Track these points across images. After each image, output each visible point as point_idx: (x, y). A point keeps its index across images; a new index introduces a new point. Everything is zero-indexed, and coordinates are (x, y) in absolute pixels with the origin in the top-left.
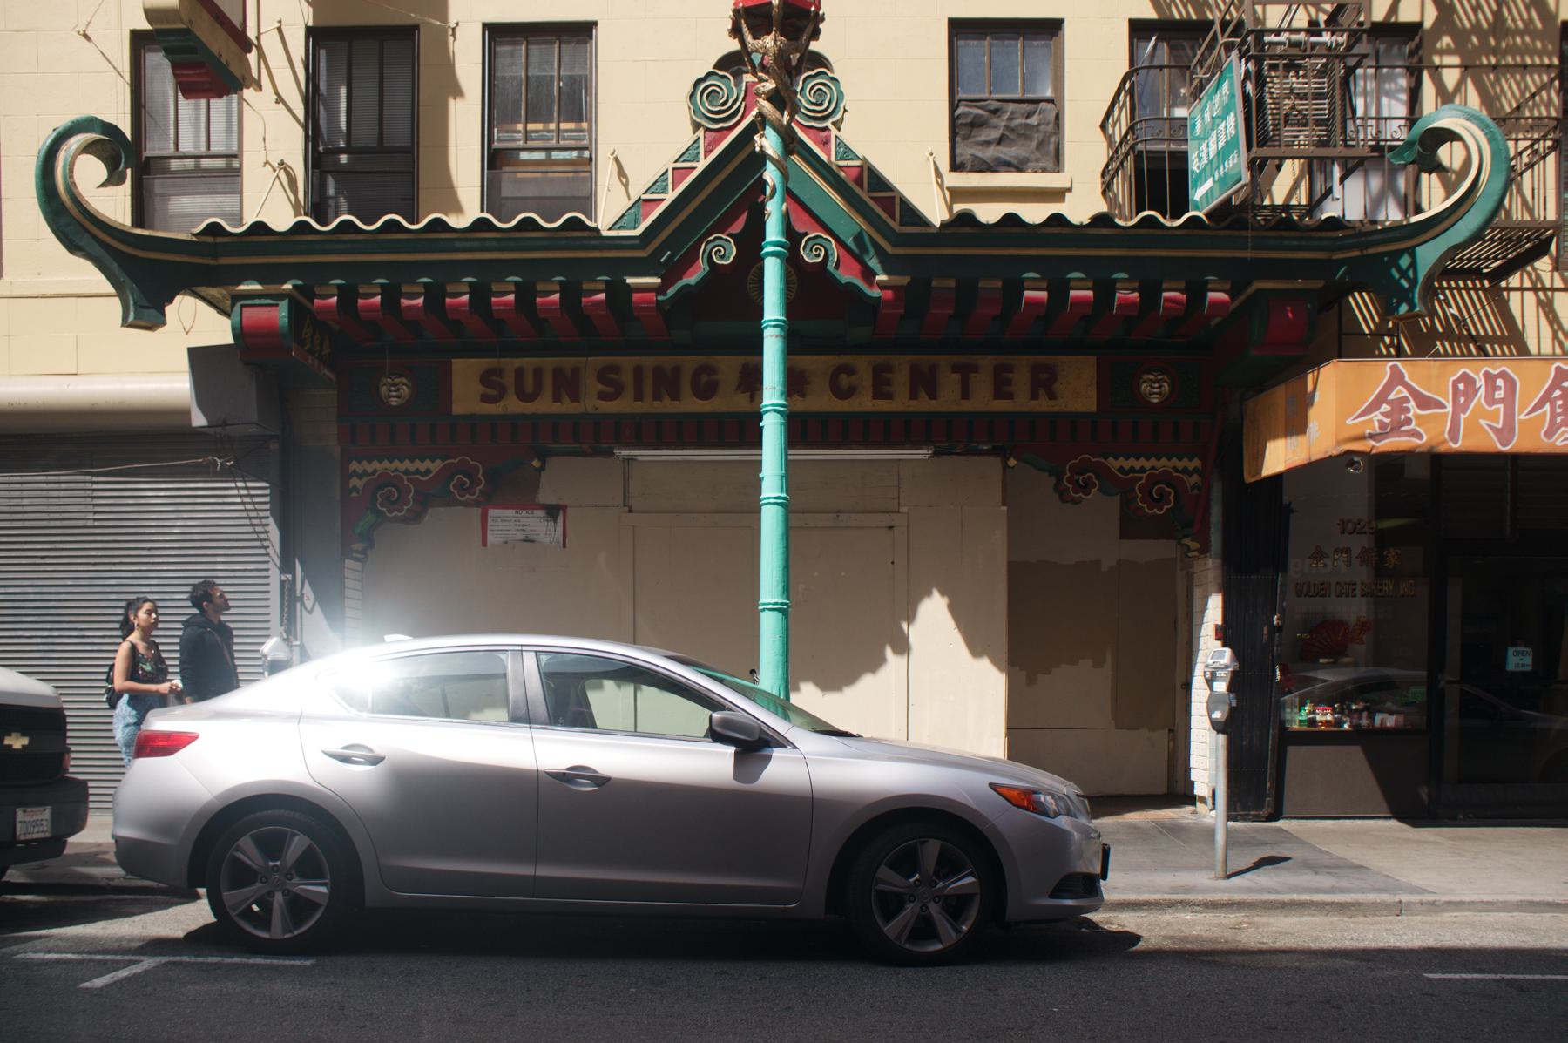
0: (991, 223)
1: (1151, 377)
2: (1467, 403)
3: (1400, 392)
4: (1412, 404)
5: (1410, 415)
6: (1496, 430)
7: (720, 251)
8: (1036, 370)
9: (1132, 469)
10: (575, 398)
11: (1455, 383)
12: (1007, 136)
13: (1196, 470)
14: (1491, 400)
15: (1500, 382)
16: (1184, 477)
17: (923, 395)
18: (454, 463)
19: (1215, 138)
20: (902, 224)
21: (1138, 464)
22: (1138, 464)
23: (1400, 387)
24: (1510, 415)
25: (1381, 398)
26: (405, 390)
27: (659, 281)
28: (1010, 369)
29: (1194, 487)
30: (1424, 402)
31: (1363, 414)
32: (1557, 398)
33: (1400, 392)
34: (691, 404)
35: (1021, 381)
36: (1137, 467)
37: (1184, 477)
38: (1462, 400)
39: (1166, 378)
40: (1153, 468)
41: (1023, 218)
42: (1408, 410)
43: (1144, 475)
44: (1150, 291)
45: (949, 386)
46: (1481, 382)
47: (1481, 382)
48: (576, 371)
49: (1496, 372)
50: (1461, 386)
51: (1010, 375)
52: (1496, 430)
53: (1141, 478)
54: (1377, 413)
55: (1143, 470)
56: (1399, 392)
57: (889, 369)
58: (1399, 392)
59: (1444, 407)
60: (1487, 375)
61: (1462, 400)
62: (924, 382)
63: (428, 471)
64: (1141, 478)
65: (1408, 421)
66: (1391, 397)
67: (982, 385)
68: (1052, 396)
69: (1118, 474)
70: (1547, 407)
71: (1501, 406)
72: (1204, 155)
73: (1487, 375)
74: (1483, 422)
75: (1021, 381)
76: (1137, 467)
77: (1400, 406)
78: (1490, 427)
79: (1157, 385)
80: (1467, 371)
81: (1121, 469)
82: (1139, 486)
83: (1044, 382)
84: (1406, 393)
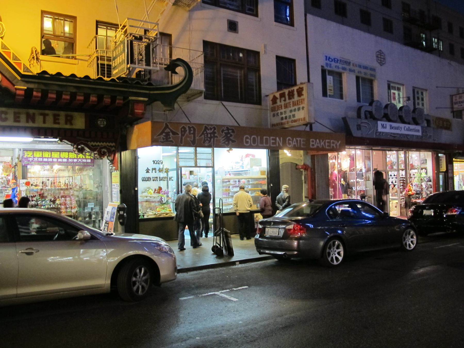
0: (53, 74)
1: (101, 120)
2: (184, 134)
3: (168, 130)
4: (171, 134)
6: (191, 141)
8: (67, 116)
9: (95, 146)
10: (34, 121)
11: (181, 129)
13: (113, 146)
14: (190, 133)
15: (192, 129)
17: (30, 121)
19: (119, 59)
20: (24, 71)
21: (97, 144)
22: (97, 144)
23: (168, 129)
24: (194, 137)
26: (105, 123)
28: (59, 115)
30: (174, 133)
31: (159, 135)
32: (205, 134)
33: (168, 130)
35: (62, 119)
37: (110, 148)
38: (183, 133)
39: (105, 120)
41: (48, 72)
43: (99, 147)
44: (113, 99)
45: (39, 119)
46: (187, 129)
47: (187, 129)
48: (34, 114)
49: (191, 126)
51: (59, 117)
52: (191, 141)
55: (98, 146)
56: (167, 130)
57: (59, 115)
58: (167, 130)
59: (178, 134)
61: (183, 133)
62: (30, 118)
64: (98, 148)
65: (170, 138)
66: (166, 131)
67: (50, 119)
68: (71, 124)
70: (203, 136)
72: (116, 62)
73: (189, 127)
75: (62, 119)
77: (167, 134)
79: (102, 122)
80: (184, 126)
81: (92, 145)
83: (69, 120)
84: (169, 131)
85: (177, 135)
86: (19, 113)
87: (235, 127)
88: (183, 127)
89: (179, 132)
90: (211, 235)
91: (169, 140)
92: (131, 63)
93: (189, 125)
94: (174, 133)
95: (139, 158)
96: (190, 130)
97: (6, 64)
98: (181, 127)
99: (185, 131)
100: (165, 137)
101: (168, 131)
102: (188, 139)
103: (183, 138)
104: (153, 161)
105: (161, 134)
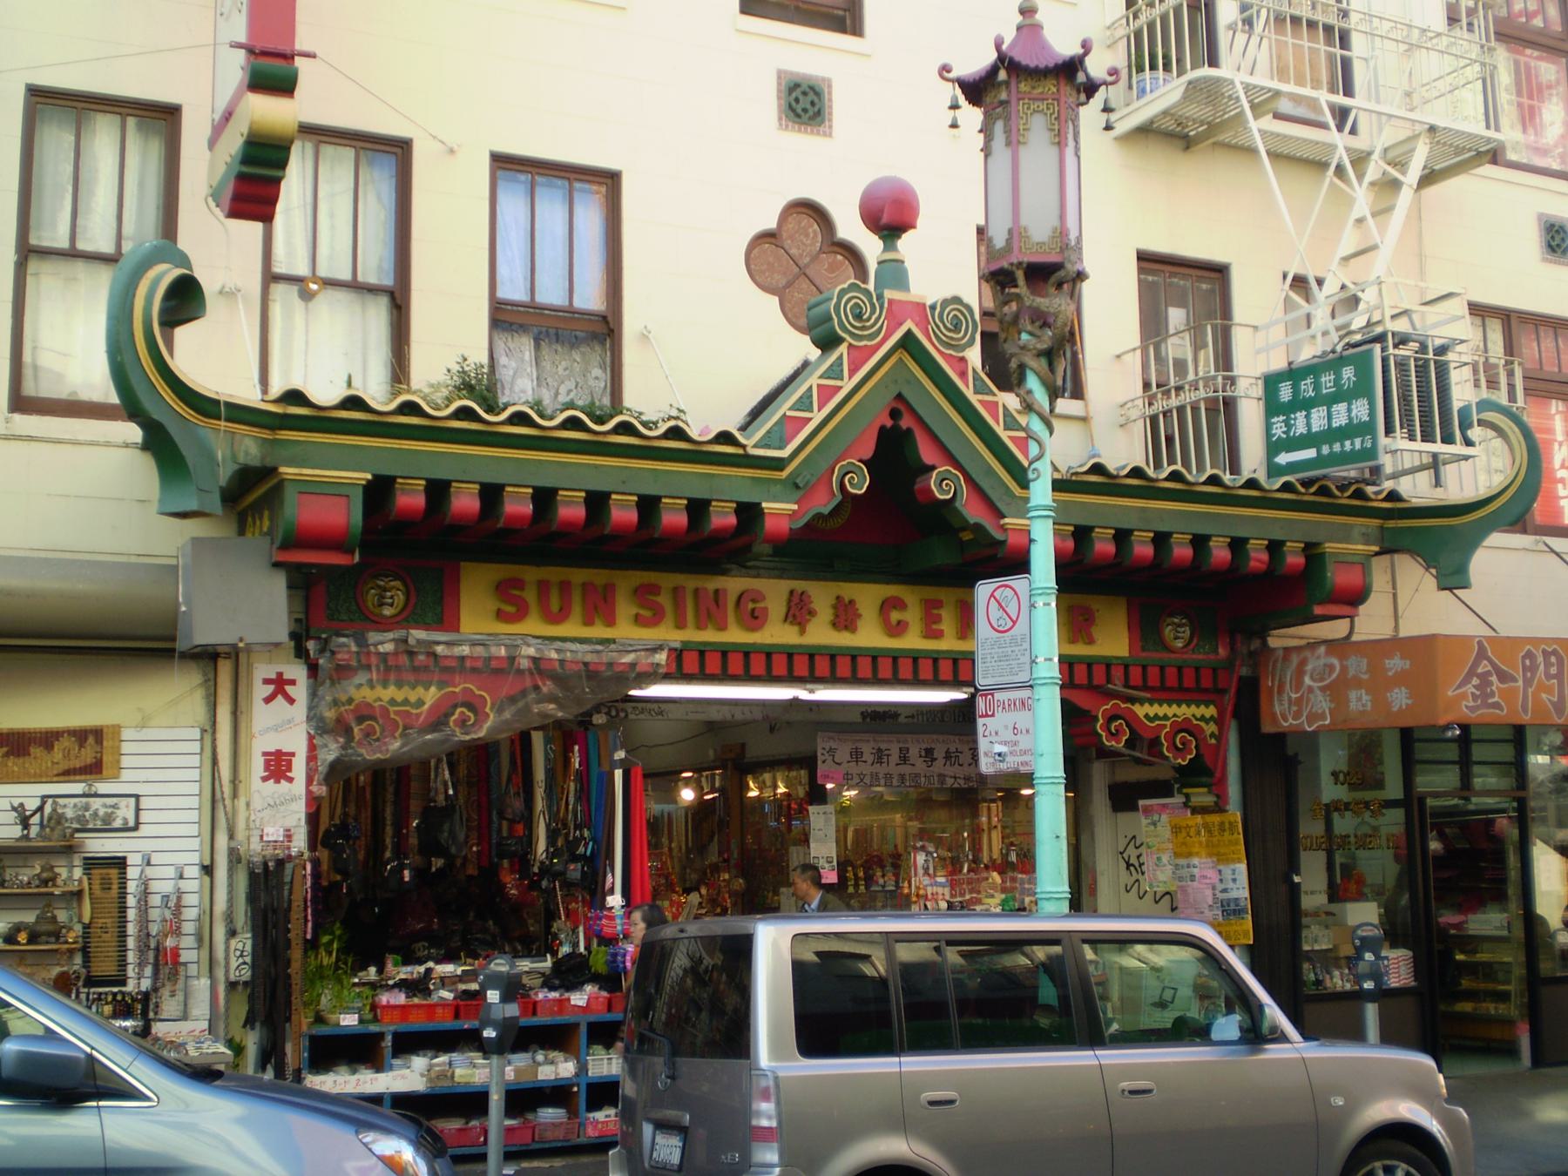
1: (1176, 620)
4: (1494, 679)
5: (1494, 688)
7: (852, 477)
9: (1156, 717)
11: (1524, 657)
12: (1337, 487)
14: (1548, 676)
15: (1553, 659)
16: (1202, 724)
18: (473, 692)
25: (1472, 673)
27: (795, 507)
29: (1212, 735)
31: (1459, 686)
34: (735, 635)
36: (1161, 714)
37: (1202, 724)
38: (1529, 674)
39: (401, 588)
40: (1175, 715)
42: (1491, 684)
43: (1168, 723)
46: (1540, 659)
49: (1550, 650)
50: (1528, 662)
53: (1165, 726)
54: (1470, 686)
55: (1166, 717)
59: (1514, 680)
60: (1544, 652)
63: (420, 703)
65: (1492, 694)
66: (1480, 670)
69: (1146, 721)
71: (1555, 681)
73: (1544, 652)
74: (1544, 696)
76: (1161, 714)
77: (1484, 680)
78: (1549, 700)
82: (484, 697)
85: (1512, 684)
86: (938, 604)
87: (1488, 638)
88: (1529, 655)
89: (1518, 674)
90: (704, 1015)
91: (1490, 701)
92: (225, 431)
93: (1543, 646)
94: (1503, 677)
95: (1300, 763)
96: (1548, 665)
97: (764, 472)
98: (1522, 654)
99: (1533, 668)
100: (1478, 693)
101: (1486, 669)
102: (1544, 696)
103: (1530, 690)
104: (1333, 774)
105: (1466, 681)
